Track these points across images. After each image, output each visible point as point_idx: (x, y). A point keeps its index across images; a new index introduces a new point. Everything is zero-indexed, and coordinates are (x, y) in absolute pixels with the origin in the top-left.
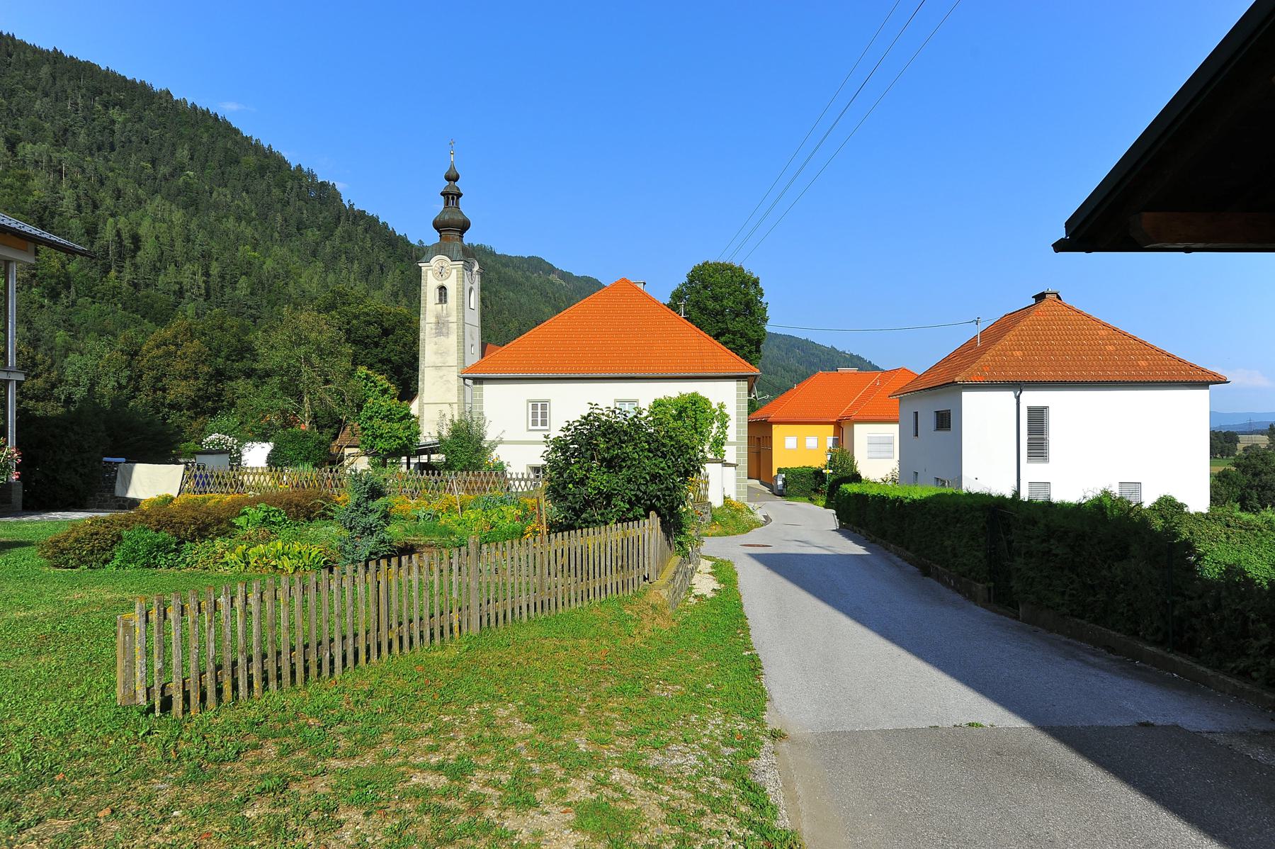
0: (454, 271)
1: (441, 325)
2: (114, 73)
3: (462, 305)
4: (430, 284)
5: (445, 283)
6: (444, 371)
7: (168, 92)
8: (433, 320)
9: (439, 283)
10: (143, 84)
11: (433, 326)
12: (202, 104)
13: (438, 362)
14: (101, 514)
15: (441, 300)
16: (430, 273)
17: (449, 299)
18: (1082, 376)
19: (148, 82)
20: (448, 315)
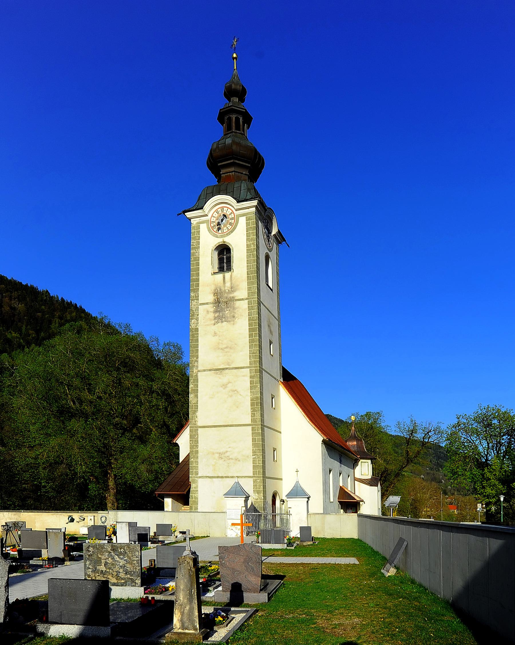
0: (243, 221)
1: (222, 303)
2: (15, 281)
3: (257, 275)
4: (206, 243)
5: (229, 240)
6: (228, 376)
7: (47, 291)
8: (211, 298)
9: (219, 241)
10: (32, 287)
11: (211, 308)
12: (68, 299)
13: (219, 361)
14: (467, 523)
15: (221, 269)
16: (203, 228)
17: (235, 263)
18: (450, 516)
19: (35, 286)
20: (233, 289)
